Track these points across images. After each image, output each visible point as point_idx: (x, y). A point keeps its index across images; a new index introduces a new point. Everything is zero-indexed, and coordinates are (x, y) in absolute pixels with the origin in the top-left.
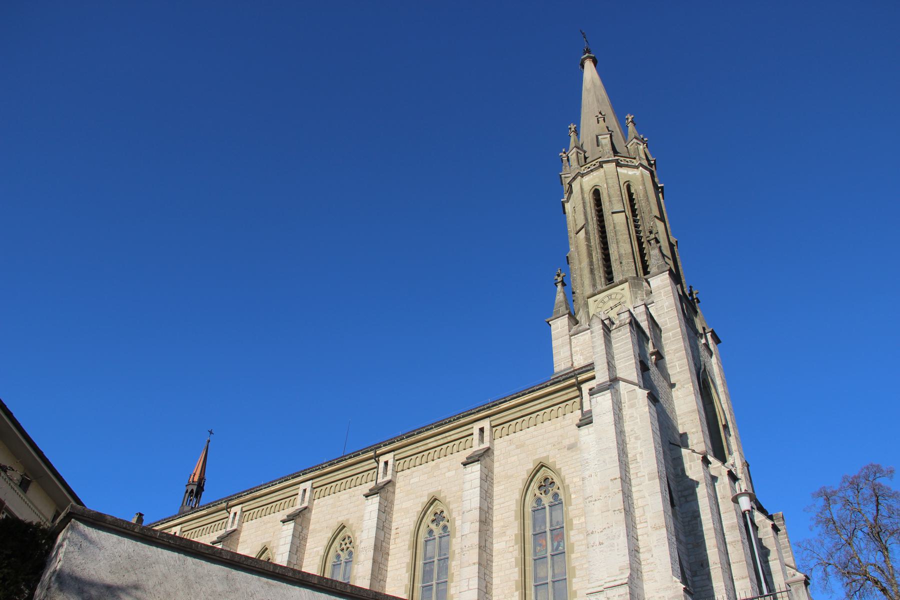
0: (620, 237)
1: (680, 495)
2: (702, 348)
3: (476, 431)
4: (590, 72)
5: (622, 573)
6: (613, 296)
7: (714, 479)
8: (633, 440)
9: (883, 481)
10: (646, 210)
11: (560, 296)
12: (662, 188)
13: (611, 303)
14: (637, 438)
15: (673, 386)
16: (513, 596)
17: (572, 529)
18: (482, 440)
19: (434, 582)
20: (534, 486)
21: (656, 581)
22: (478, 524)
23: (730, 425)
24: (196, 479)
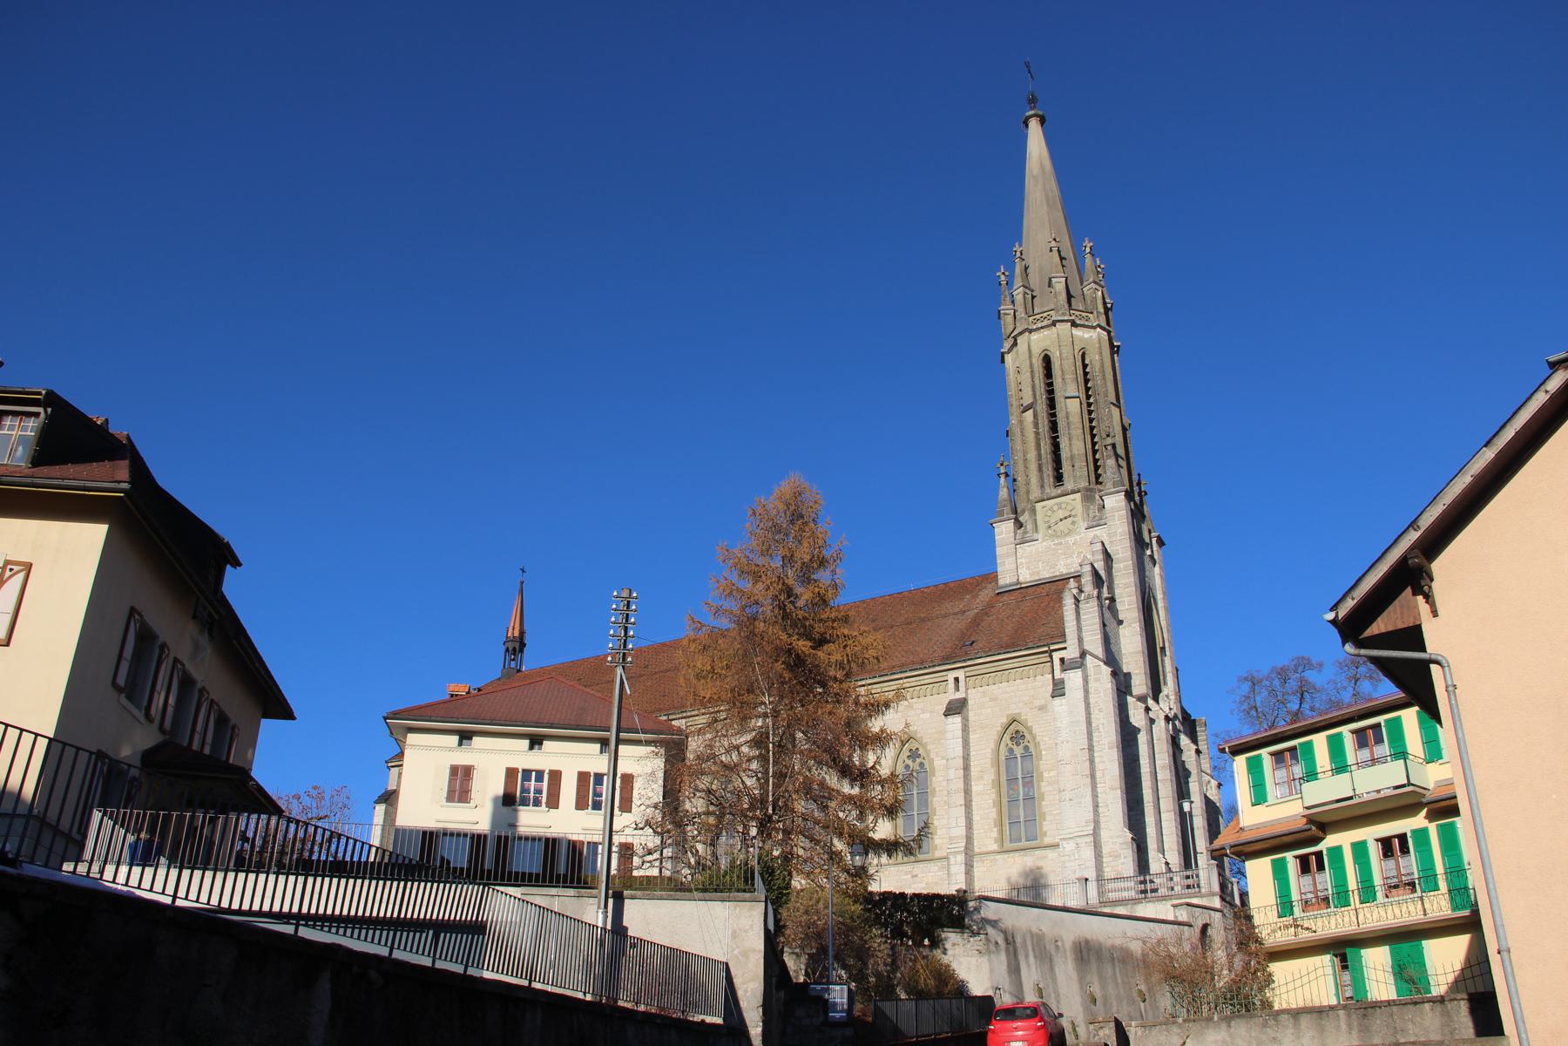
0: (1073, 432)
1: (1128, 736)
2: (1147, 560)
3: (951, 681)
4: (1035, 131)
7: (1152, 721)
9: (1310, 675)
10: (1101, 390)
11: (1003, 493)
13: (1061, 514)
15: (1121, 622)
18: (957, 689)
24: (517, 634)
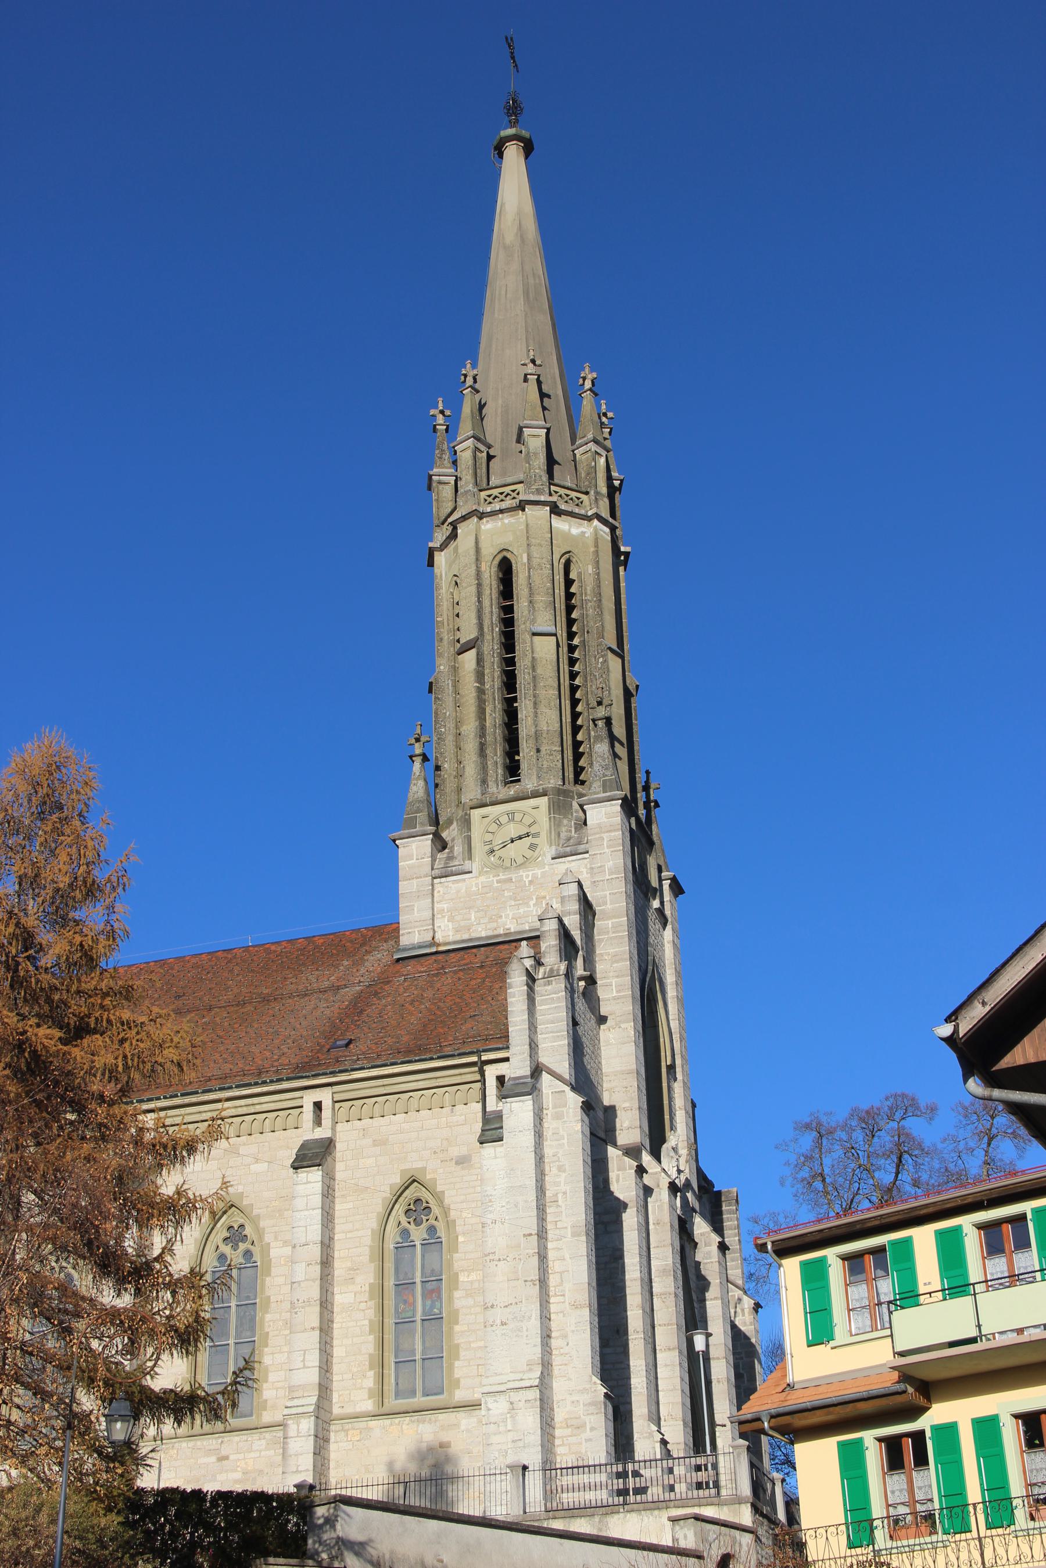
0: (542, 693)
2: (652, 916)
5: (530, 1370)
6: (518, 817)
7: (648, 1191)
8: (554, 1170)
9: (915, 1125)
10: (593, 625)
11: (417, 789)
12: (627, 554)
14: (561, 1169)
15: (602, 1020)
16: (365, 1376)
17: (457, 1289)
18: (318, 1121)
19: (231, 1342)
20: (399, 1209)
21: (569, 1379)
22: (319, 1267)
23: (679, 1070)
